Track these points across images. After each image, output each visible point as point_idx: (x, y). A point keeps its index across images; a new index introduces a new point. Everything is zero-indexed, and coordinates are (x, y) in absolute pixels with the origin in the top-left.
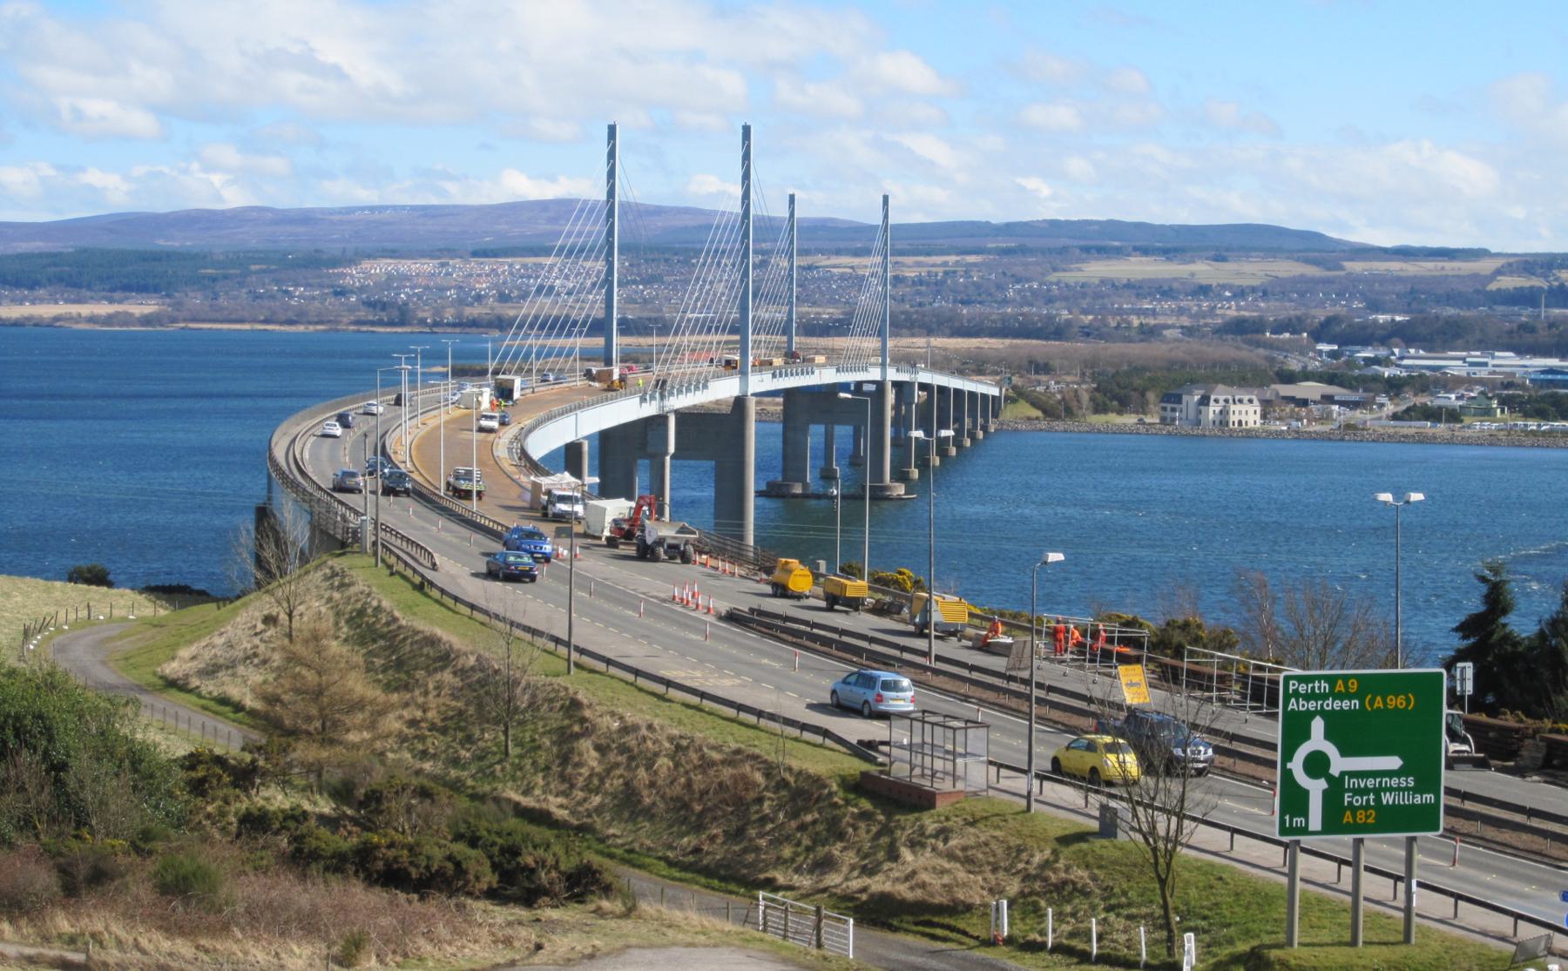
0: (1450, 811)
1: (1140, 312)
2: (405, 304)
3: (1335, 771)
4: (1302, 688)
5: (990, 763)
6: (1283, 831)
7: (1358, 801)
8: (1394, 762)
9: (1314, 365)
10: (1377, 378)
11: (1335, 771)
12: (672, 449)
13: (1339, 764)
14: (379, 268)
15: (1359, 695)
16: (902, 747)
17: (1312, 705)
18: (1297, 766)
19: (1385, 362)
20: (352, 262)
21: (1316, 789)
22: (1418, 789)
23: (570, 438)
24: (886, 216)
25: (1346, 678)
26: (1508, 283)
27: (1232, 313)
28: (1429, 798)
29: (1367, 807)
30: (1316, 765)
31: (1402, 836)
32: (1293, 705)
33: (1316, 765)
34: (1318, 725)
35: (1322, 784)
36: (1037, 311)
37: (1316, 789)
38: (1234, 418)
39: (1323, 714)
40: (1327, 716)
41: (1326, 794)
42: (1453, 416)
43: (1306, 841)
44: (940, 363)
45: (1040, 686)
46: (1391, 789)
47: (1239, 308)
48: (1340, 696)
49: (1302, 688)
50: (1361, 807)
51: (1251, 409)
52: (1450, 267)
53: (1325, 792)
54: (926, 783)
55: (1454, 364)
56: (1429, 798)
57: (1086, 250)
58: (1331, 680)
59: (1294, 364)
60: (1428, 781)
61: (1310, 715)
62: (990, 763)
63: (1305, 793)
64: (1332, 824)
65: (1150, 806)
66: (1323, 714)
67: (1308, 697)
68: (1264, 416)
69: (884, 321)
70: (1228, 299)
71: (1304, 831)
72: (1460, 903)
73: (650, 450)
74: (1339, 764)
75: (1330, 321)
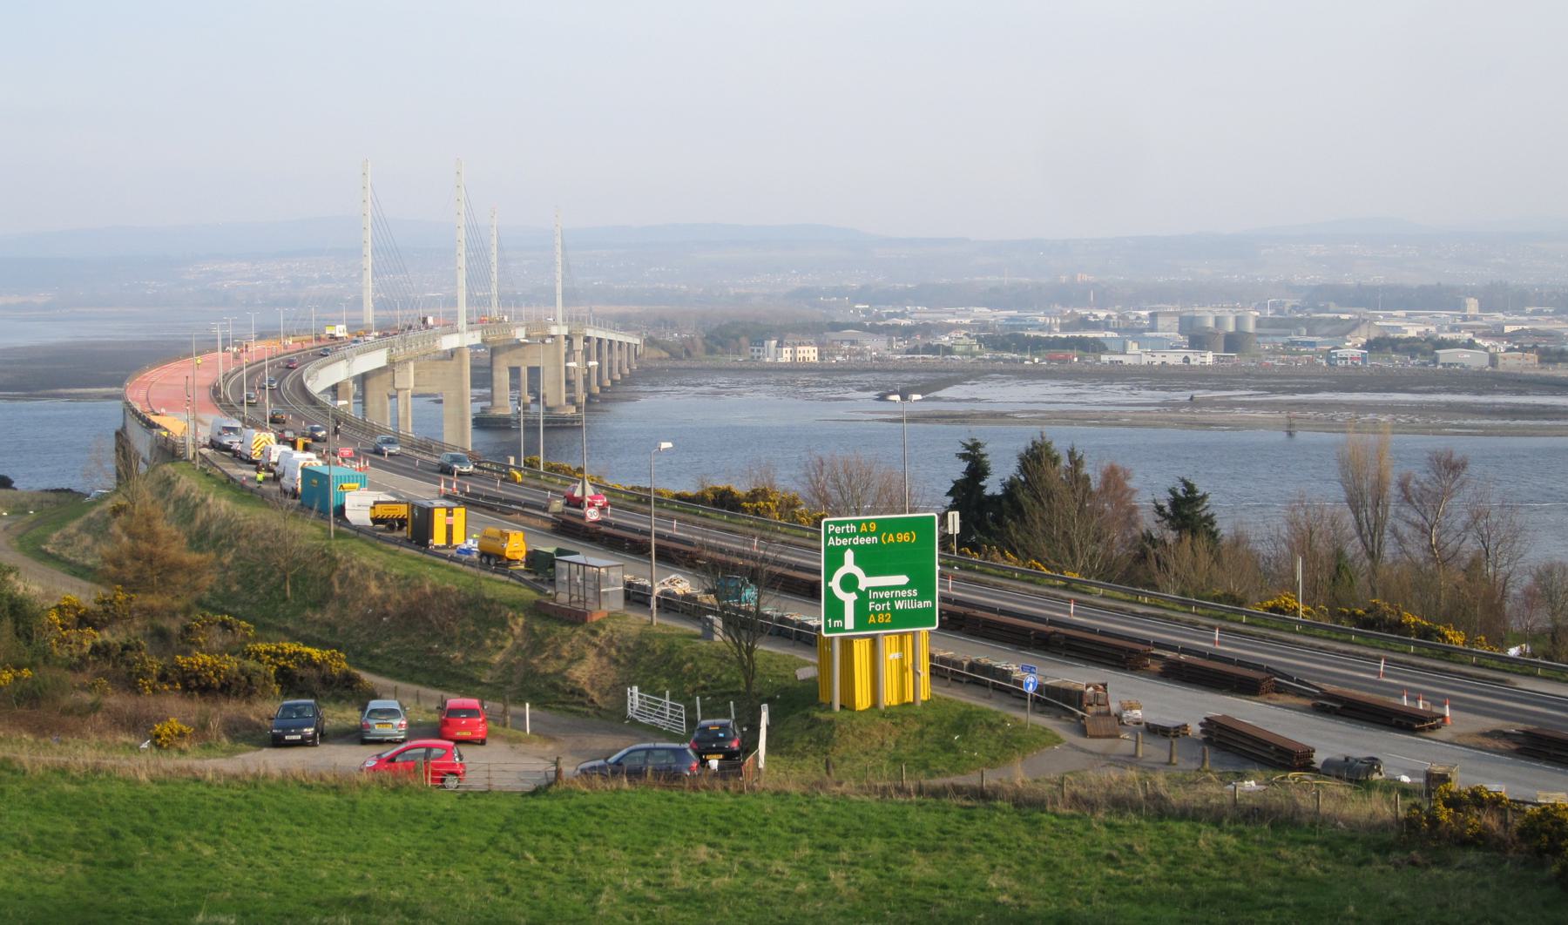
3: (862, 587)
4: (838, 530)
7: (878, 607)
8: (903, 580)
11: (862, 587)
15: (878, 533)
17: (845, 542)
18: (835, 584)
19: (903, 316)
21: (849, 599)
22: (920, 598)
23: (455, 345)
25: (868, 522)
28: (928, 603)
29: (886, 611)
30: (849, 583)
32: (831, 541)
33: (849, 583)
34: (849, 556)
35: (853, 596)
37: (849, 599)
38: (800, 356)
39: (852, 547)
46: (901, 598)
48: (865, 535)
49: (838, 530)
51: (811, 349)
54: (580, 607)
56: (928, 603)
58: (858, 524)
61: (844, 548)
66: (852, 547)
67: (841, 536)
71: (842, 629)
74: (865, 582)
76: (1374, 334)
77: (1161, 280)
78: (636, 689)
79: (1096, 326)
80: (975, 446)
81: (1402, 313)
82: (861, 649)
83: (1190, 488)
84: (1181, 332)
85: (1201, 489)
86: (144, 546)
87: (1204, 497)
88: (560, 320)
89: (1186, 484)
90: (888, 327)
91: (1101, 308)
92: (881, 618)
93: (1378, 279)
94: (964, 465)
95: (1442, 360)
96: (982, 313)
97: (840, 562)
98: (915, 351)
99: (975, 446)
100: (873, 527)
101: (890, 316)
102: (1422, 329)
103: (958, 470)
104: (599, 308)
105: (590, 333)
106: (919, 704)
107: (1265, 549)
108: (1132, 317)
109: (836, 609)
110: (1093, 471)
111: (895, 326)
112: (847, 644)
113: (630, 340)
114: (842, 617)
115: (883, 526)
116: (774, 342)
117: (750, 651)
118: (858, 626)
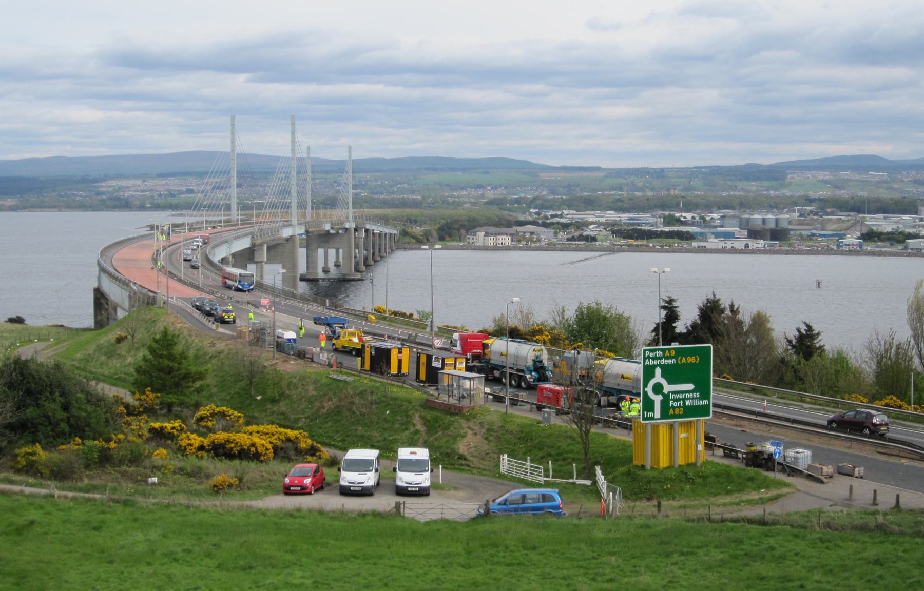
0: (715, 405)
1: (452, 196)
2: (128, 198)
3: (665, 391)
4: (651, 355)
7: (676, 404)
8: (691, 387)
11: (665, 391)
13: (667, 388)
14: (115, 183)
17: (655, 362)
18: (649, 389)
19: (561, 216)
20: (104, 180)
21: (657, 399)
22: (701, 398)
25: (670, 350)
26: (609, 181)
28: (706, 402)
29: (680, 407)
30: (658, 389)
32: (647, 362)
33: (658, 389)
34: (658, 371)
35: (660, 397)
37: (657, 399)
39: (660, 366)
41: (662, 401)
46: (689, 399)
48: (667, 358)
49: (651, 355)
51: (506, 237)
52: (585, 174)
56: (706, 402)
57: (427, 169)
58: (663, 351)
59: (522, 218)
60: (705, 395)
61: (654, 367)
63: (653, 402)
64: (665, 414)
66: (660, 366)
67: (653, 359)
68: (512, 241)
71: (653, 418)
75: (535, 199)
76: (865, 231)
77: (724, 194)
78: (506, 456)
79: (685, 223)
80: (671, 301)
81: (881, 216)
82: (664, 433)
83: (809, 328)
85: (816, 329)
86: (166, 362)
87: (818, 334)
88: (351, 218)
89: (808, 326)
90: (553, 223)
91: (688, 211)
93: (864, 194)
94: (664, 313)
95: (911, 246)
96: (612, 215)
97: (653, 376)
99: (671, 301)
100: (673, 353)
101: (553, 216)
102: (895, 227)
103: (659, 316)
105: (368, 227)
106: (698, 465)
109: (648, 405)
110: (746, 317)
111: (558, 223)
112: (656, 428)
114: (652, 410)
116: (483, 233)
117: (587, 432)
118: (663, 417)
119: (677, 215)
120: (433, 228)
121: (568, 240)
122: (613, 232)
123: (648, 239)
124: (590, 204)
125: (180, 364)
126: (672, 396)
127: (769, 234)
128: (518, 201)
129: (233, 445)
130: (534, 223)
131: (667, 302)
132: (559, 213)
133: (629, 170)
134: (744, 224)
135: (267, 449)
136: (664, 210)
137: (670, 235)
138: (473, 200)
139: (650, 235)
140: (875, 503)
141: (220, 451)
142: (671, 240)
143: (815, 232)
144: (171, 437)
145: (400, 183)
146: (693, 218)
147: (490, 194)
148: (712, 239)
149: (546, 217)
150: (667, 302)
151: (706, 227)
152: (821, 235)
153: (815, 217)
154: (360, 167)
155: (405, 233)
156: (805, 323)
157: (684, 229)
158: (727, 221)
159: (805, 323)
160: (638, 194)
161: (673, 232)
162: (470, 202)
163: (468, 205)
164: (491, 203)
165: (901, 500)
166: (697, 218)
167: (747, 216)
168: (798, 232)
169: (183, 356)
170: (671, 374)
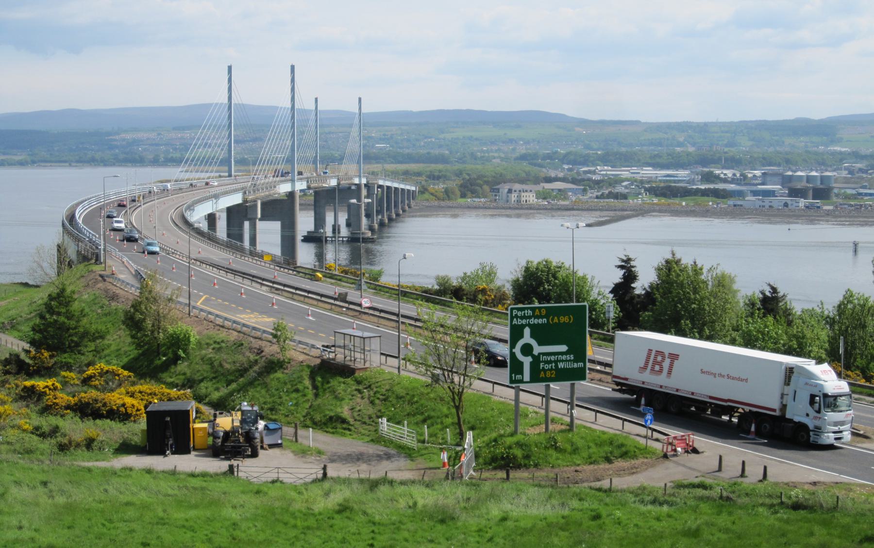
1: (483, 151)
3: (536, 352)
5: (382, 354)
6: (512, 381)
7: (547, 367)
8: (563, 348)
9: (561, 175)
10: (589, 180)
11: (536, 352)
12: (259, 216)
13: (537, 349)
15: (546, 316)
16: (340, 347)
17: (524, 322)
18: (517, 350)
19: (594, 173)
21: (527, 361)
22: (576, 360)
24: (360, 108)
27: (524, 151)
28: (581, 364)
29: (551, 369)
30: (527, 350)
31: (568, 383)
32: (515, 322)
33: (527, 350)
34: (527, 331)
35: (530, 359)
36: (436, 152)
37: (527, 361)
38: (523, 199)
39: (529, 325)
40: (532, 327)
42: (624, 197)
43: (522, 386)
44: (394, 175)
45: (403, 316)
46: (563, 361)
47: (527, 149)
48: (538, 317)
49: (519, 314)
50: (548, 370)
53: (531, 363)
54: (351, 364)
55: (624, 173)
59: (553, 174)
61: (523, 327)
62: (382, 354)
63: (522, 364)
65: (451, 371)
66: (529, 325)
67: (522, 318)
69: (360, 156)
70: (522, 145)
71: (522, 381)
72: (598, 414)
73: (249, 216)
74: (537, 349)
78: (385, 419)
79: (725, 181)
83: (774, 290)
84: (782, 185)
92: (548, 374)
94: (621, 273)
96: (648, 172)
97: (522, 336)
98: (602, 197)
99: (628, 260)
100: (544, 312)
103: (617, 276)
104: (390, 167)
105: (381, 182)
107: (348, 249)
108: (750, 175)
113: (408, 187)
114: (522, 373)
115: (550, 312)
119: (717, 172)
120: (453, 184)
121: (597, 197)
122: (646, 190)
123: (681, 196)
124: (627, 159)
125: (78, 321)
126: (542, 358)
127: (811, 193)
128: (549, 157)
129: (100, 405)
130: (564, 180)
131: (623, 261)
132: (593, 169)
133: (105, 165)
134: (786, 181)
135: (138, 410)
136: (704, 166)
137: (705, 193)
138: (503, 155)
139: (686, 193)
140: (743, 475)
141: (86, 411)
142: (706, 198)
143: (862, 191)
144: (41, 395)
145: (426, 138)
146: (734, 175)
147: (522, 150)
148: (750, 198)
149: (578, 173)
150: (623, 261)
151: (746, 184)
152: (866, 195)
153: (864, 176)
154: (364, 120)
155: (423, 190)
156: (769, 285)
157: (721, 186)
158: (768, 179)
159: (769, 285)
160: (678, 149)
161: (709, 189)
162: (499, 157)
163: (498, 161)
164: (523, 157)
165: (747, 468)
166: (738, 175)
167: (790, 173)
168: (843, 191)
169: (736, 292)
170: (543, 335)
